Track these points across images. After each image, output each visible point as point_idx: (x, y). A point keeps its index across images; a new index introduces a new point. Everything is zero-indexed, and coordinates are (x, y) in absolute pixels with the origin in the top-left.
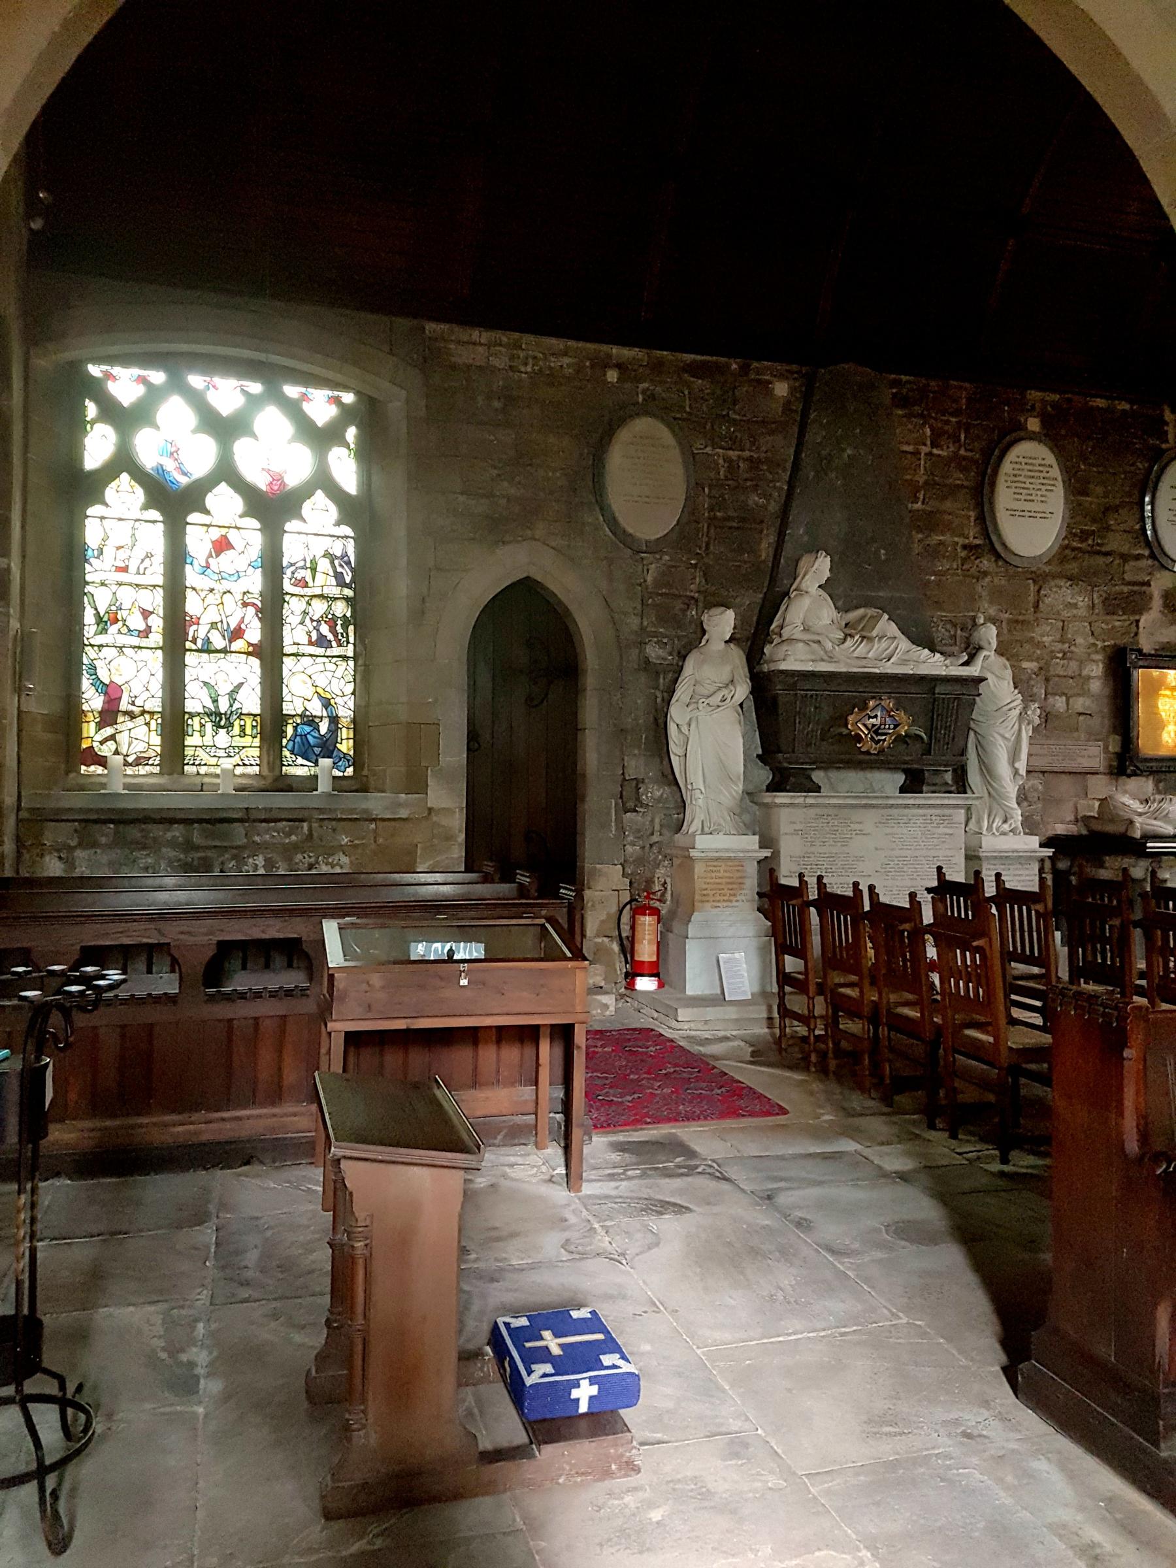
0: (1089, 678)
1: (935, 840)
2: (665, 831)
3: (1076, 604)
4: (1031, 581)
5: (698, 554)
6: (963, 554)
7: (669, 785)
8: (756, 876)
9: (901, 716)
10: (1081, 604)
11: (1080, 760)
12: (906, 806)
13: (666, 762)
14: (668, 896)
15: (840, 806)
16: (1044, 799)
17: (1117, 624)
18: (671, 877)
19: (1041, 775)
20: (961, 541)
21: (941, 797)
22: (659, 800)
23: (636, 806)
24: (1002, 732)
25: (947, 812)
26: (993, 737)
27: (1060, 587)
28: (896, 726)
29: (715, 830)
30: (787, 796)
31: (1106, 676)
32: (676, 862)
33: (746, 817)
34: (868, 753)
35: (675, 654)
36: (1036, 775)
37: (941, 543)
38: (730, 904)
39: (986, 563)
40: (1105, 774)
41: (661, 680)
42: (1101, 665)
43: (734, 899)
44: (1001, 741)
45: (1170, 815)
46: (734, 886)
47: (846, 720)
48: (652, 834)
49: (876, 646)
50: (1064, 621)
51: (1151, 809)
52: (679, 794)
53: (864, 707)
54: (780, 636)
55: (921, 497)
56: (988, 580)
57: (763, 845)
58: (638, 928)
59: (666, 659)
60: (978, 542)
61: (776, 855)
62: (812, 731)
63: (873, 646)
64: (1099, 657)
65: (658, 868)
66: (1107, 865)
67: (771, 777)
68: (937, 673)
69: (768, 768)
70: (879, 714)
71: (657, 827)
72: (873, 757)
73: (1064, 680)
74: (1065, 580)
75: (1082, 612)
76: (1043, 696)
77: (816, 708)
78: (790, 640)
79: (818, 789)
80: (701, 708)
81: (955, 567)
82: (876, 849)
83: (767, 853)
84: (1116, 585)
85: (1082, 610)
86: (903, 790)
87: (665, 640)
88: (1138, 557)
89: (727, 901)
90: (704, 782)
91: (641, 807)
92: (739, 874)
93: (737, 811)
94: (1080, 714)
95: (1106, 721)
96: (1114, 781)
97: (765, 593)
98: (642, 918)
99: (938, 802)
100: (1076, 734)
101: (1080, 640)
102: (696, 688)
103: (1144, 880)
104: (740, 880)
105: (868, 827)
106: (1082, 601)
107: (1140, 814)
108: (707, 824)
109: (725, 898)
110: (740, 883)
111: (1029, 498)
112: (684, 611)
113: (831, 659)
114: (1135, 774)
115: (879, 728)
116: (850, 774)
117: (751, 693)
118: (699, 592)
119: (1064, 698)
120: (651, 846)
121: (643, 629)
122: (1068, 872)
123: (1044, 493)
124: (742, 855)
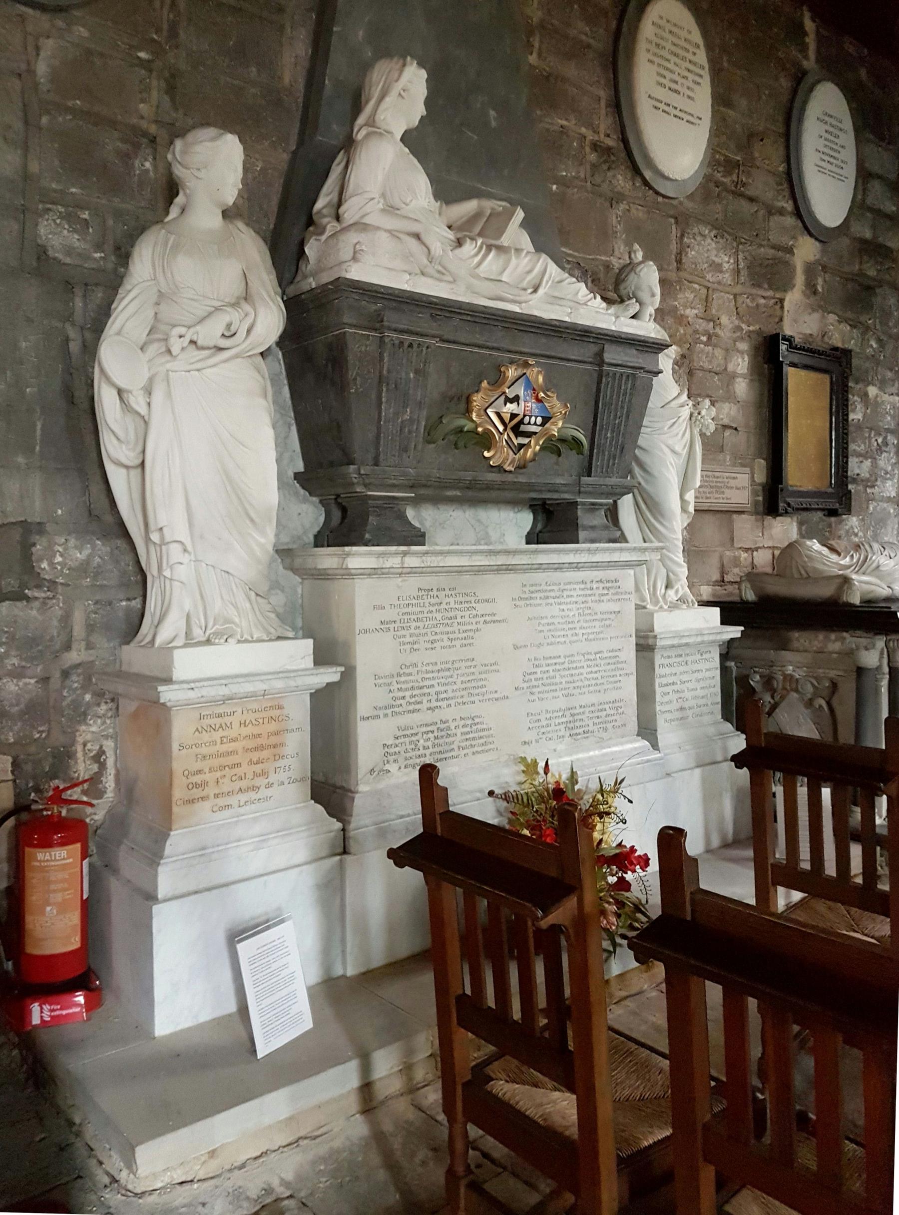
0: (733, 376)
1: (597, 624)
2: (100, 641)
3: (720, 265)
4: (673, 221)
5: (153, 40)
6: (593, 157)
7: (105, 536)
8: (308, 728)
9: (555, 405)
10: (726, 266)
12: (540, 567)
13: (96, 488)
14: (109, 781)
15: (460, 571)
17: (762, 301)
18: (115, 737)
20: (590, 136)
21: (608, 549)
22: (83, 569)
23: (23, 586)
24: (670, 442)
25: (612, 574)
26: (662, 450)
27: (704, 236)
28: (546, 420)
29: (217, 634)
30: (370, 554)
31: (751, 375)
32: (129, 707)
33: (279, 599)
34: (500, 469)
35: (109, 247)
37: (563, 130)
38: (253, 795)
39: (621, 181)
41: (79, 303)
42: (746, 358)
43: (261, 782)
44: (670, 458)
45: (881, 568)
46: (265, 754)
47: (468, 401)
48: (68, 647)
49: (514, 261)
50: (708, 288)
52: (129, 558)
53: (498, 380)
54: (338, 218)
55: (537, 45)
56: (623, 206)
57: (322, 658)
58: (33, 880)
59: (88, 258)
60: (610, 142)
61: (349, 675)
62: (411, 420)
63: (509, 260)
64: (743, 346)
65: (84, 721)
66: (796, 644)
67: (322, 519)
68: (604, 326)
69: (315, 500)
70: (521, 394)
71: (79, 630)
72: (510, 478)
73: (708, 375)
74: (709, 227)
75: (727, 278)
77: (417, 372)
78: (361, 226)
79: (417, 538)
80: (175, 350)
81: (582, 175)
82: (516, 647)
83: (330, 675)
84: (761, 246)
85: (727, 275)
86: (533, 538)
87: (85, 215)
88: (781, 212)
89: (248, 789)
90: (191, 524)
91: (38, 587)
92: (273, 727)
93: (263, 588)
97: (294, 153)
98: (42, 856)
99: (606, 557)
100: (721, 456)
101: (724, 320)
102: (163, 307)
103: (879, 668)
104: (273, 740)
105: (503, 608)
106: (726, 261)
108: (198, 620)
109: (243, 784)
110: (275, 746)
111: (674, 86)
112: (126, 158)
113: (442, 273)
115: (521, 422)
116: (455, 514)
117: (280, 343)
118: (156, 122)
120: (66, 674)
121: (26, 177)
123: (691, 85)
124: (279, 684)
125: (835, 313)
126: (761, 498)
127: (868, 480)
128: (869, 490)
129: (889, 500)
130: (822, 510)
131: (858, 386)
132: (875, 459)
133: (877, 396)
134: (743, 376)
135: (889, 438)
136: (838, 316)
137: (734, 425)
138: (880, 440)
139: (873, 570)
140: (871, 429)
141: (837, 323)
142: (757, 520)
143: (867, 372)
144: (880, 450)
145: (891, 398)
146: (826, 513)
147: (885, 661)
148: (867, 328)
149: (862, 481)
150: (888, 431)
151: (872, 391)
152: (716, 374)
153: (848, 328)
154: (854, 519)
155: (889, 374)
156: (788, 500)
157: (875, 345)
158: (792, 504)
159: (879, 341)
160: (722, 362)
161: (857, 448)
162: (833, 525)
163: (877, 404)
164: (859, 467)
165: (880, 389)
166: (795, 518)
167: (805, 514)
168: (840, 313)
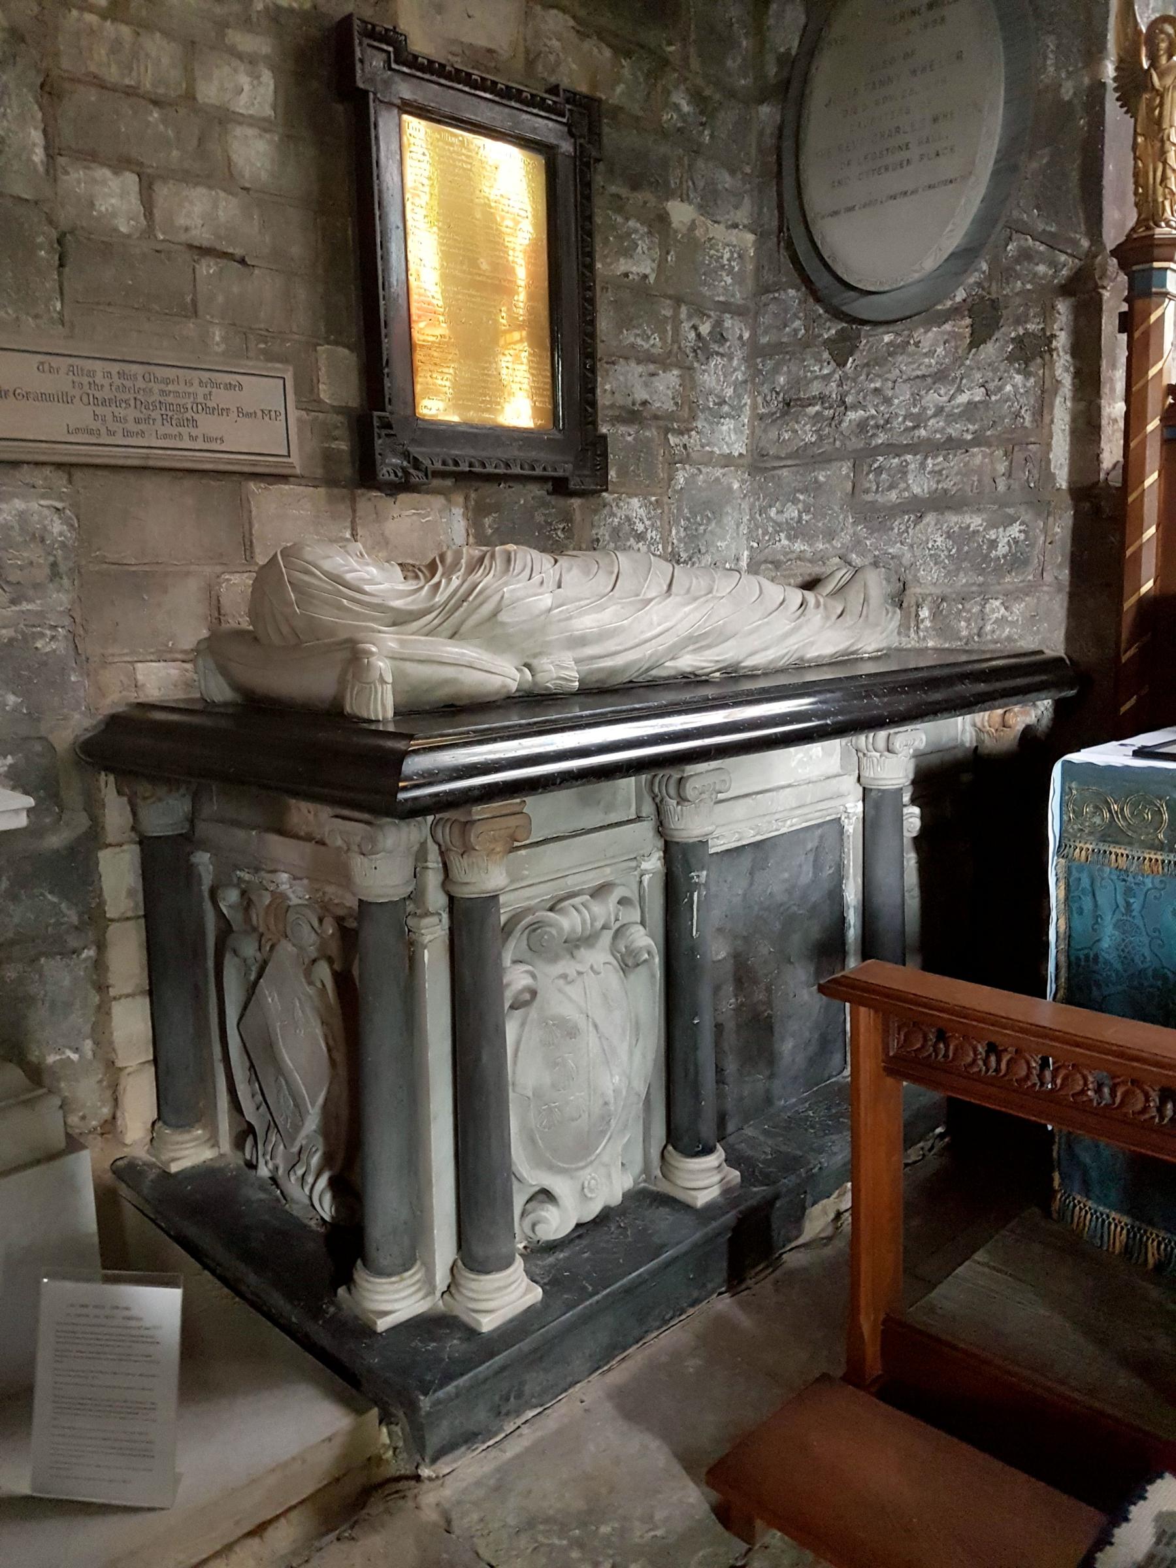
0: (223, 118)
11: (208, 424)
16: (76, 571)
19: (59, 480)
36: (38, 477)
40: (315, 483)
42: (267, 77)
45: (503, 617)
51: (440, 598)
76: (39, 155)
94: (205, 251)
95: (302, 294)
96: (343, 508)
100: (190, 328)
107: (400, 619)
114: (401, 486)
119: (131, 179)
122: (186, 841)
125: (564, 10)
126: (344, 446)
127: (671, 417)
128: (673, 440)
129: (727, 461)
130: (542, 479)
131: (640, 196)
132: (691, 368)
133: (693, 226)
134: (264, 125)
135: (728, 323)
136: (574, 17)
137: (238, 252)
138: (705, 329)
139: (479, 624)
140: (678, 301)
141: (573, 36)
142: (331, 500)
143: (664, 163)
144: (703, 350)
145: (733, 236)
146: (549, 486)
147: (433, 879)
148: (664, 63)
149: (656, 417)
150: (725, 307)
151: (681, 213)
152: (156, 103)
153: (608, 53)
154: (635, 502)
155: (726, 180)
156: (415, 450)
157: (686, 108)
158: (426, 462)
159: (697, 97)
160: (175, 74)
161: (639, 341)
162: (578, 516)
163: (692, 245)
164: (646, 385)
165: (703, 209)
166: (460, 499)
167: (489, 489)
168: (582, 13)
